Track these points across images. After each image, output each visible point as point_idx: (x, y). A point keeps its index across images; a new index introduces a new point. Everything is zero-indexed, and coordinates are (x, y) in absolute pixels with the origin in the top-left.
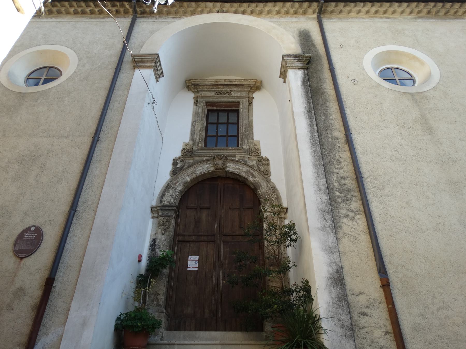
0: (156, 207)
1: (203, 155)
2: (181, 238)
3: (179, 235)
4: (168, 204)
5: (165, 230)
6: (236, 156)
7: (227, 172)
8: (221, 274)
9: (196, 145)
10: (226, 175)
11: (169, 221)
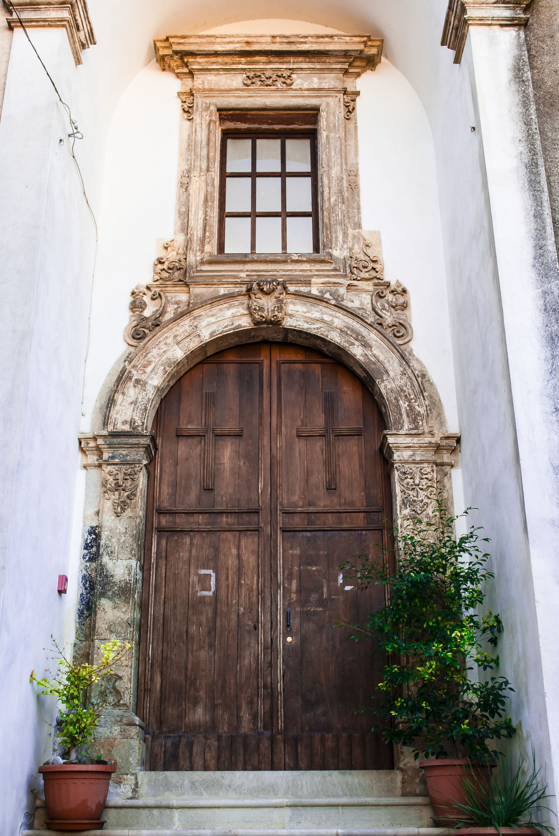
0: (95, 438)
1: (220, 281)
2: (164, 521)
3: (161, 512)
4: (127, 428)
5: (124, 502)
6: (314, 280)
7: (287, 331)
8: (280, 617)
9: (196, 245)
10: (286, 336)
11: (131, 476)
